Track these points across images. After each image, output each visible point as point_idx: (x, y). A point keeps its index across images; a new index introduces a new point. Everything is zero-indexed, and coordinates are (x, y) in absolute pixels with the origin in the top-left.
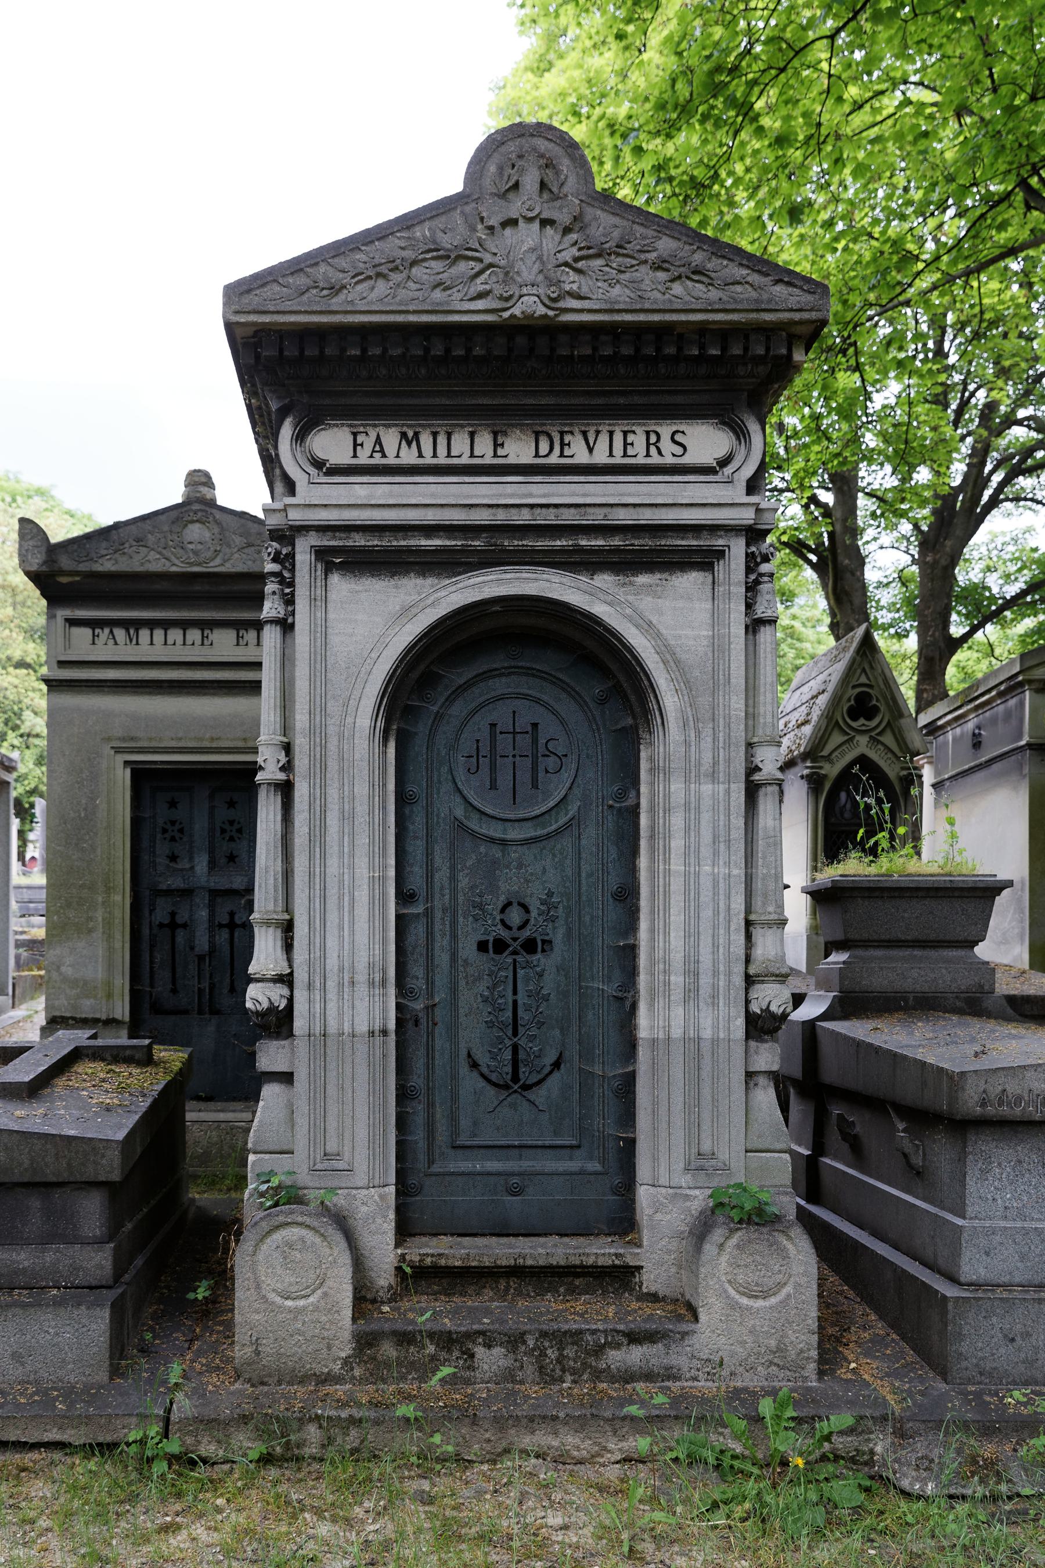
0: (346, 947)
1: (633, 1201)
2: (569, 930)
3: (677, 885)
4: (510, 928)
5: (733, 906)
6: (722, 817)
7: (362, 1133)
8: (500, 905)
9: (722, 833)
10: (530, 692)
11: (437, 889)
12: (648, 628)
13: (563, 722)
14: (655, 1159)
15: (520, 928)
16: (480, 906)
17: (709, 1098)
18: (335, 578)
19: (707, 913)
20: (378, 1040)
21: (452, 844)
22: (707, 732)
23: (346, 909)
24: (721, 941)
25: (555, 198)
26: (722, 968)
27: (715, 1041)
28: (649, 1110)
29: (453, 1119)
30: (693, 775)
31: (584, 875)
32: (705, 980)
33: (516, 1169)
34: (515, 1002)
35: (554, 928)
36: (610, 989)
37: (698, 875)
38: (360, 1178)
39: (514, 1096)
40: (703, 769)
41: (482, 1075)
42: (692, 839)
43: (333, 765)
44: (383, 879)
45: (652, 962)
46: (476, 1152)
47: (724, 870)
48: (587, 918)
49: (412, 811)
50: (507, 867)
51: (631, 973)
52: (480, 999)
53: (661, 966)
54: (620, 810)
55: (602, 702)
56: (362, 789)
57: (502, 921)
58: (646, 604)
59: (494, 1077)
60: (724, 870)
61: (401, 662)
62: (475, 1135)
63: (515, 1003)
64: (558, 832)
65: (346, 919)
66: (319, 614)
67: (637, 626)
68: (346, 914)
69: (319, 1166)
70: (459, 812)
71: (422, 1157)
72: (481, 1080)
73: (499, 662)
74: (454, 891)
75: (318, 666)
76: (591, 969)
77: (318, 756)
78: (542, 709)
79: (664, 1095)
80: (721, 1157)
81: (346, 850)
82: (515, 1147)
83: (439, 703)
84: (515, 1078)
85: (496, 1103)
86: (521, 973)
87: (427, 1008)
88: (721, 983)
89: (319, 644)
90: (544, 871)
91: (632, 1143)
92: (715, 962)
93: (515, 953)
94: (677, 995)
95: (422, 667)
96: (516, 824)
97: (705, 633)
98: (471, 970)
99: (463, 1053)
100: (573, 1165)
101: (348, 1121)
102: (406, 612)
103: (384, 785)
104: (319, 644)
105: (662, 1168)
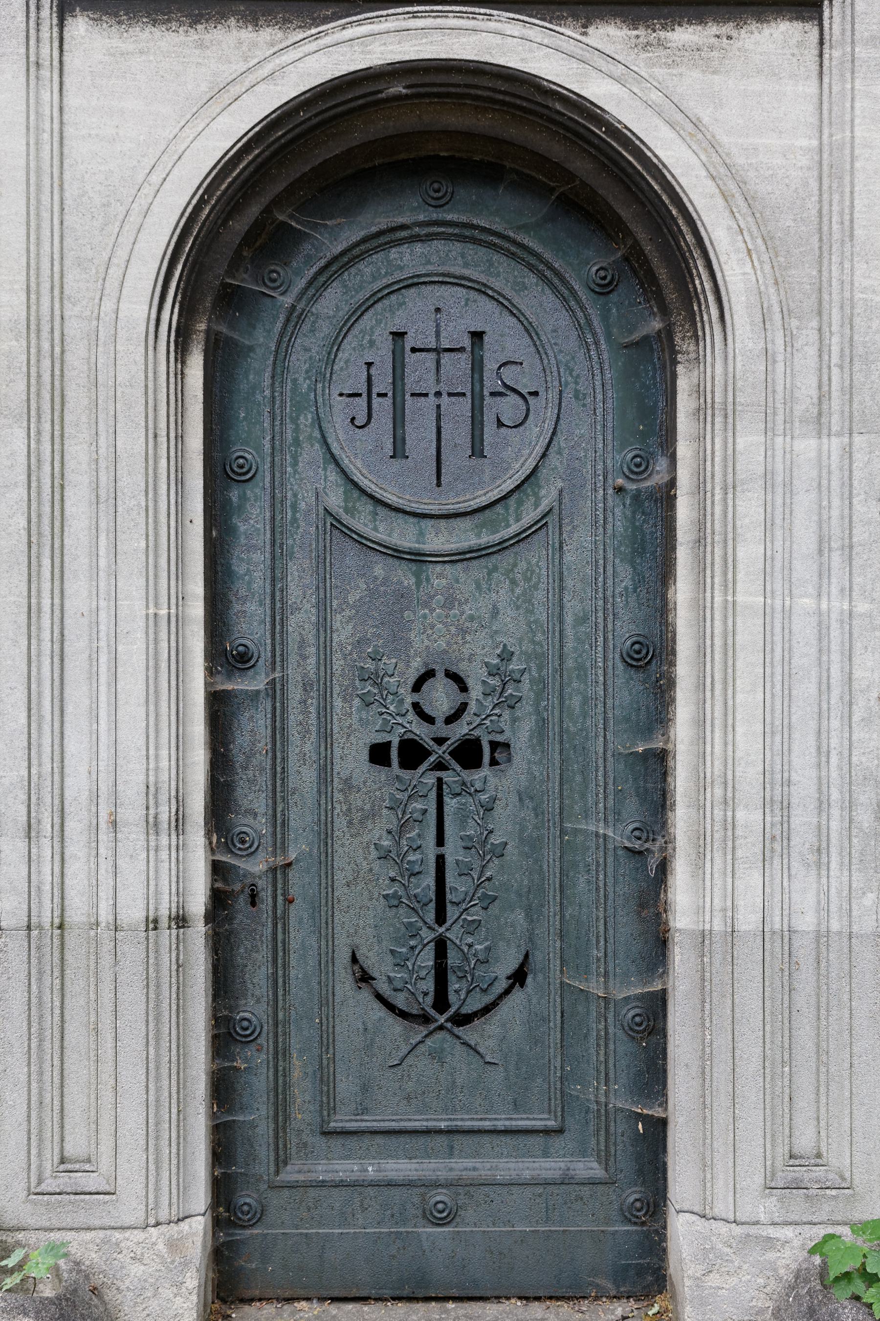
0: (103, 754)
1: (663, 1238)
2: (542, 725)
3: (748, 632)
4: (430, 720)
5: (857, 674)
6: (836, 502)
7: (133, 1119)
8: (412, 676)
9: (836, 531)
10: (466, 272)
11: (292, 646)
12: (694, 129)
13: (529, 330)
14: (705, 1165)
15: (450, 720)
16: (376, 679)
17: (810, 1045)
18: (79, 26)
19: (806, 690)
20: (167, 936)
22: (808, 336)
23: (103, 679)
24: (834, 742)
26: (835, 795)
27: (821, 937)
28: (695, 1070)
29: (325, 1079)
30: (780, 418)
31: (569, 619)
32: (803, 819)
33: (443, 1175)
34: (440, 861)
35: (514, 720)
36: (619, 835)
37: (788, 613)
38: (130, 1207)
40: (799, 409)
41: (379, 997)
42: (778, 544)
43: (77, 396)
44: (178, 622)
45: (701, 784)
46: (366, 1140)
47: (838, 605)
48: (576, 702)
49: (243, 498)
50: (426, 605)
51: (658, 804)
52: (374, 854)
53: (718, 791)
54: (637, 497)
55: (604, 289)
56: (132, 442)
57: (416, 706)
58: (689, 83)
59: (400, 1001)
60: (838, 605)
61: (210, 190)
62: (365, 1111)
64: (521, 538)
65: (103, 698)
66: (46, 96)
67: (671, 125)
68: (103, 689)
69: (49, 1185)
70: (335, 500)
71: (264, 1152)
72: (377, 1005)
73: (409, 210)
75: (45, 198)
76: (583, 796)
77: (46, 378)
78: (491, 305)
79: (722, 1041)
80: (834, 1162)
81: (103, 563)
82: (440, 1132)
83: (296, 290)
84: (441, 1002)
85: (405, 1049)
86: (451, 804)
87: (273, 870)
88: (834, 825)
89: (46, 154)
90: (495, 613)
91: (658, 1128)
92: (823, 786)
93: (440, 766)
94: (749, 847)
95: (254, 210)
96: (443, 523)
97: (804, 142)
98: (357, 799)
99: (343, 957)
100: (549, 1167)
101: (107, 1095)
102: (221, 94)
103: (180, 438)
104: (46, 154)
105: (720, 1183)
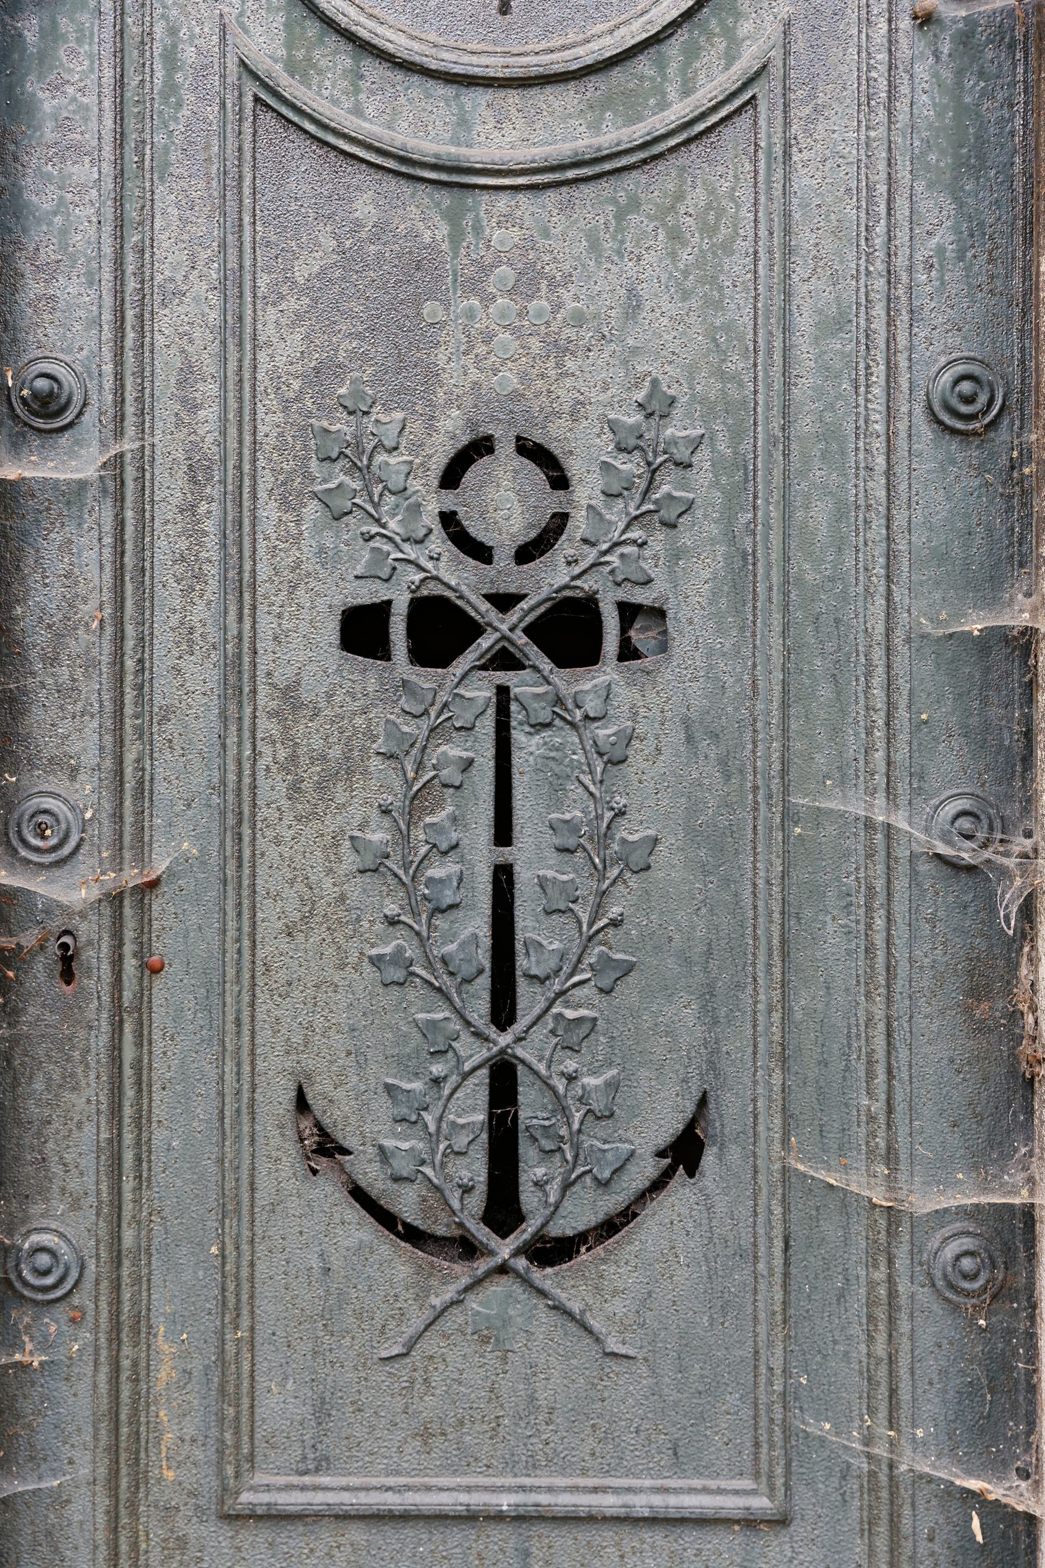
2: (743, 564)
4: (481, 553)
15: (526, 554)
21: (230, 182)
25: (576, 561)
29: (231, 1392)
31: (804, 321)
34: (503, 879)
35: (676, 555)
36: (924, 827)
39: (500, 1287)
41: (359, 1195)
48: (819, 515)
50: (474, 286)
52: (350, 861)
57: (448, 519)
63: (503, 879)
64: (694, 133)
72: (354, 1213)
74: (240, 392)
76: (836, 731)
82: (499, 1517)
84: (503, 1208)
85: (416, 1321)
86: (527, 747)
90: (633, 305)
93: (505, 659)
96: (513, 97)
98: (311, 735)
